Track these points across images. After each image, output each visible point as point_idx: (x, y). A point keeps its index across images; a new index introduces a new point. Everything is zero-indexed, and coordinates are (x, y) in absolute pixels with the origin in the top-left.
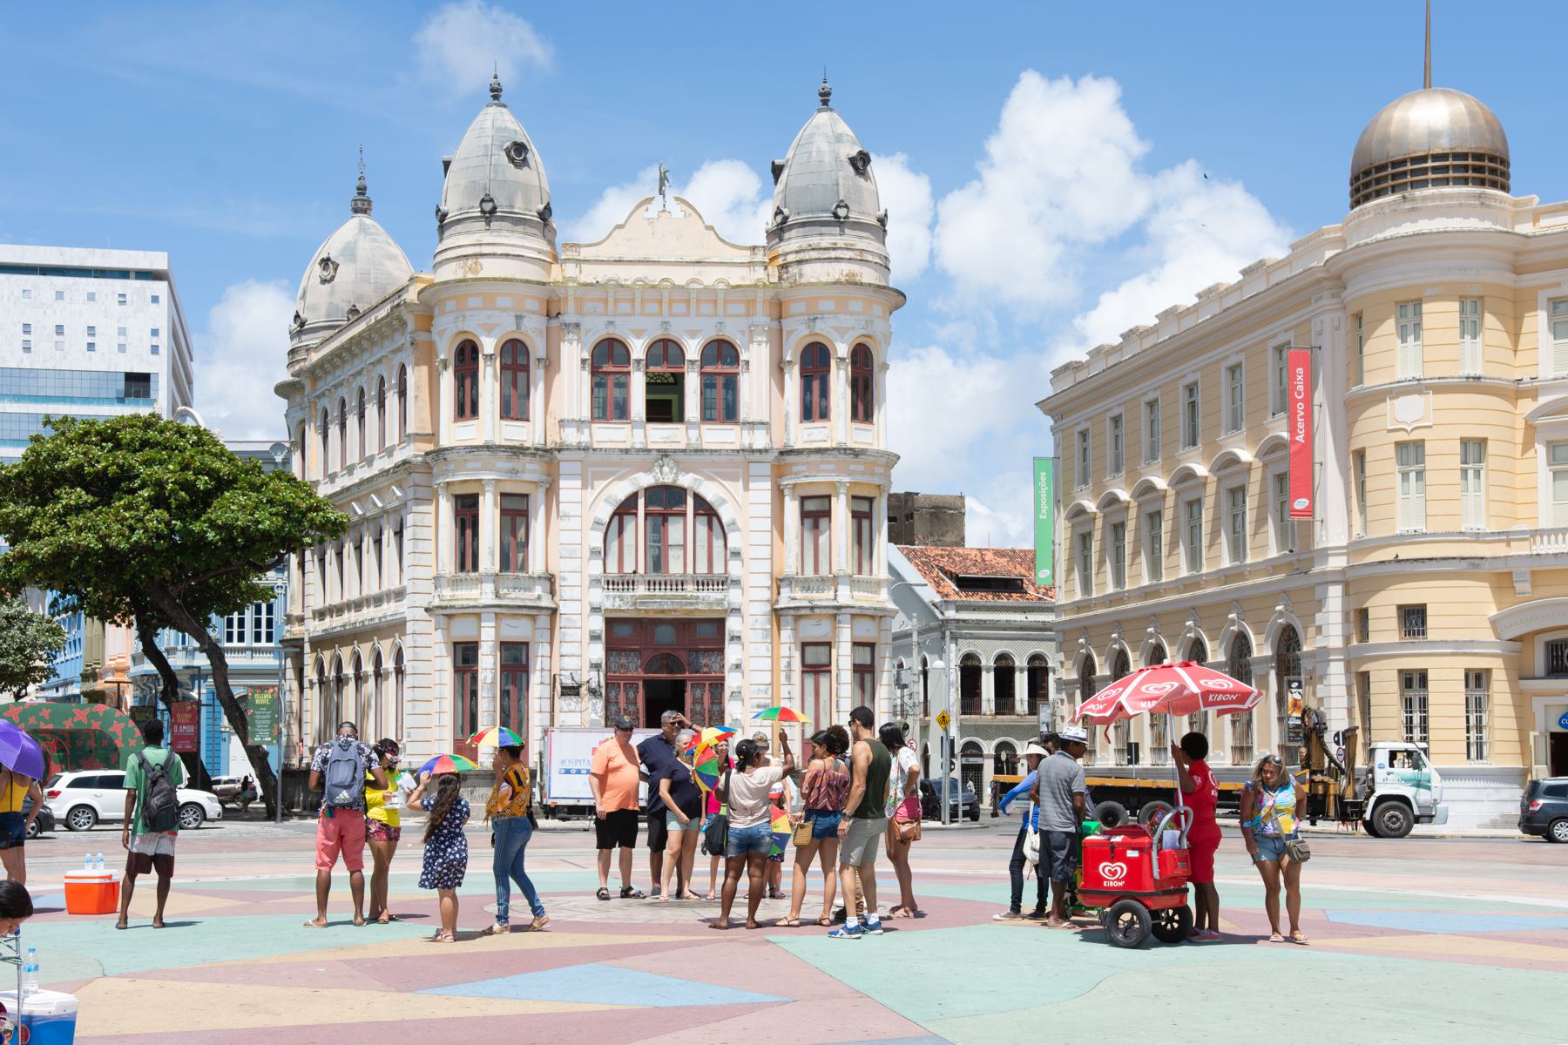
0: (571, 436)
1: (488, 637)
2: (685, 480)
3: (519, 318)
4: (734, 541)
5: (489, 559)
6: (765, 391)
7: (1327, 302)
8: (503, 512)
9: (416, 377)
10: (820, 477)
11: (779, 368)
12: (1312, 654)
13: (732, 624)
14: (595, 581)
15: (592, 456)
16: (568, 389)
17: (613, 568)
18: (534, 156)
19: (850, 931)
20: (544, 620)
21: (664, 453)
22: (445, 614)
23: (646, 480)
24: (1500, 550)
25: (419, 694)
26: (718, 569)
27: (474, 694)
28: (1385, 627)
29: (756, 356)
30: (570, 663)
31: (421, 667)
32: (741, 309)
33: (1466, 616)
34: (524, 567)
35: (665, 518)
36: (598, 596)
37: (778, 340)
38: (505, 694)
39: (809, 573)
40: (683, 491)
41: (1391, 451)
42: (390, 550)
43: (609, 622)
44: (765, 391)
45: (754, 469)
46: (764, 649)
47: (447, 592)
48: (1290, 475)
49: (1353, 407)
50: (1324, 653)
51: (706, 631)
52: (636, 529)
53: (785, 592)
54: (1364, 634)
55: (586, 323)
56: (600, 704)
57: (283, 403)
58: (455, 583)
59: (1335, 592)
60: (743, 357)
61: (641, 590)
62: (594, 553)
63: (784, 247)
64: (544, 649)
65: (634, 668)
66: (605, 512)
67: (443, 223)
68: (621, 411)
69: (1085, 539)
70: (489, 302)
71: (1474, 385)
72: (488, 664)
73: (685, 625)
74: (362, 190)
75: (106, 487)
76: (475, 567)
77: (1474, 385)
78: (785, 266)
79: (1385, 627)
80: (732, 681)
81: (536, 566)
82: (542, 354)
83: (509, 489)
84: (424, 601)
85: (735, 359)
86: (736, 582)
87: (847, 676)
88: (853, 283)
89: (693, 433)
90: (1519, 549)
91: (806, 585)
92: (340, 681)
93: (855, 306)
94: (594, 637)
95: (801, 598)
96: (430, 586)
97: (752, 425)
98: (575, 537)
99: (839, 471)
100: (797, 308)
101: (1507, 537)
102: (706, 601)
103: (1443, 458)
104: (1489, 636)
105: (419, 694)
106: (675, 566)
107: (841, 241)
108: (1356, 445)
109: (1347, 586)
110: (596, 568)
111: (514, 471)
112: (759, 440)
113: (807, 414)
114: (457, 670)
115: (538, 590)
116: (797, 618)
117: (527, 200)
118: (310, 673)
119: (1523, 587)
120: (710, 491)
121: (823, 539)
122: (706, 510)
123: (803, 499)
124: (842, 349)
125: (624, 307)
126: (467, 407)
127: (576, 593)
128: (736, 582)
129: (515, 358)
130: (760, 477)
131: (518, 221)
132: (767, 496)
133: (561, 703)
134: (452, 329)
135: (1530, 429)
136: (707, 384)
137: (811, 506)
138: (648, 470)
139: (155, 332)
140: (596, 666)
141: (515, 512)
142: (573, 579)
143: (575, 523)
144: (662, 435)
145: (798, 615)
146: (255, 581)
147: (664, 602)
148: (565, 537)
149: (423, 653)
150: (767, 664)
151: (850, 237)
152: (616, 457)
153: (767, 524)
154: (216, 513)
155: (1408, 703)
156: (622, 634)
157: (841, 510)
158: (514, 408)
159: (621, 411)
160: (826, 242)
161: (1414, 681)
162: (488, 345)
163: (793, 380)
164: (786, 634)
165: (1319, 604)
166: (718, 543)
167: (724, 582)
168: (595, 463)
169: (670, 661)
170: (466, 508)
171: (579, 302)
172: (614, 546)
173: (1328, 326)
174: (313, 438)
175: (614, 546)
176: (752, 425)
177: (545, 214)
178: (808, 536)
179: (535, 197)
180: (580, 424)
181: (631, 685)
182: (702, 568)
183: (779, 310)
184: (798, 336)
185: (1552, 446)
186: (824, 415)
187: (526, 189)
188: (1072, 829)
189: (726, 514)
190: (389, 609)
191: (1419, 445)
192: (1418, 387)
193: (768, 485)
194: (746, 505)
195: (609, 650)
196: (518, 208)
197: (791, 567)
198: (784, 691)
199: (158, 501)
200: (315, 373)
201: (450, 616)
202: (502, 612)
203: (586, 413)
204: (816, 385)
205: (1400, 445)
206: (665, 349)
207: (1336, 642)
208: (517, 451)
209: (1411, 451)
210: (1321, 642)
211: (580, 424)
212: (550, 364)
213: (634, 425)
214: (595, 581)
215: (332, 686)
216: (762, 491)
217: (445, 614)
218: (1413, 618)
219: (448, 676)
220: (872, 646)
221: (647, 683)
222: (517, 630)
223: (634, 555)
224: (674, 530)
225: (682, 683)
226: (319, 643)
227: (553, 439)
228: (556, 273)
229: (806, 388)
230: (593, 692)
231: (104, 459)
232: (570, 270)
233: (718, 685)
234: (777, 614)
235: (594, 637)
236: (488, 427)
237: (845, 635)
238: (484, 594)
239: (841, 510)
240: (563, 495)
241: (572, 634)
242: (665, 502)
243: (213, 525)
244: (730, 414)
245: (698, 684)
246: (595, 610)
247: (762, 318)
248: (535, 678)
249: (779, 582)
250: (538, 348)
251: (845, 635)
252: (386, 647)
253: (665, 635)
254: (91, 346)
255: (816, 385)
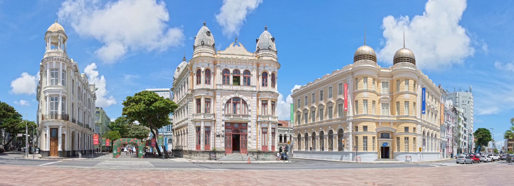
0: (219, 87)
1: (202, 125)
2: (240, 96)
3: (209, 64)
4: (249, 108)
5: (203, 111)
6: (255, 81)
7: (350, 76)
8: (205, 102)
9: (190, 78)
10: (267, 96)
11: (258, 76)
12: (346, 133)
13: (249, 124)
14: (223, 115)
15: (223, 91)
16: (217, 79)
17: (226, 113)
18: (211, 34)
20: (213, 123)
21: (236, 91)
22: (194, 121)
23: (233, 96)
24: (377, 118)
25: (190, 137)
26: (246, 113)
27: (200, 136)
28: (361, 130)
29: (254, 73)
30: (218, 131)
31: (191, 132)
32: (251, 64)
33: (372, 128)
34: (209, 112)
35: (236, 103)
36: (223, 118)
37: (258, 71)
38: (206, 136)
39: (263, 115)
40: (240, 98)
41: (362, 101)
42: (186, 112)
43: (226, 123)
44: (255, 81)
45: (253, 95)
46: (255, 129)
47: (195, 117)
48: (341, 105)
49: (354, 94)
50: (349, 133)
51: (244, 125)
52: (231, 105)
53: (259, 118)
54: (357, 130)
55: (222, 66)
56: (224, 138)
58: (196, 115)
59: (351, 123)
60: (251, 73)
61: (232, 117)
62: (223, 110)
63: (259, 54)
64: (213, 128)
65: (230, 132)
66: (225, 102)
67: (194, 47)
68: (228, 83)
69: (299, 116)
70: (203, 61)
71: (374, 92)
72: (202, 130)
73: (240, 124)
75: (137, 102)
76: (200, 112)
77: (374, 92)
78: (259, 57)
79: (361, 130)
80: (249, 134)
81: (212, 112)
82: (213, 71)
83: (207, 97)
84: (191, 120)
85: (250, 74)
86: (250, 116)
87: (271, 134)
88: (272, 60)
89: (242, 88)
90: (380, 118)
91: (263, 117)
92: (179, 135)
93: (272, 65)
94: (223, 126)
95: (262, 119)
96: (192, 117)
97: (253, 86)
98: (219, 107)
99: (269, 96)
100: (262, 65)
101: (378, 116)
102: (244, 119)
103: (370, 103)
104: (375, 131)
105: (190, 137)
106: (238, 113)
107: (270, 53)
108: (356, 99)
109: (353, 122)
110: (223, 112)
111: (207, 94)
112: (254, 89)
113: (263, 85)
114: (197, 132)
115: (212, 117)
116: (261, 123)
117: (210, 42)
118: (175, 134)
119: (380, 124)
120: (245, 98)
121: (266, 108)
122: (244, 102)
123: (262, 101)
124: (270, 73)
125: (229, 63)
126: (199, 82)
127: (219, 117)
128: (250, 116)
129: (208, 72)
130: (254, 96)
131: (208, 46)
132: (256, 100)
133: (216, 138)
134: (196, 67)
135: (379, 100)
136: (245, 78)
137: (264, 102)
138: (233, 94)
140: (223, 131)
141: (208, 101)
142: (219, 115)
143: (219, 104)
144: (236, 88)
145: (261, 122)
147: (236, 119)
148: (217, 107)
149: (191, 129)
150: (255, 131)
151: (271, 53)
152: (227, 91)
153: (256, 105)
154: (154, 105)
155: (364, 142)
156: (228, 125)
157: (269, 103)
158: (208, 82)
159: (228, 83)
160: (267, 53)
161: (365, 138)
162: (203, 69)
163: (261, 79)
164: (259, 126)
165: (348, 125)
166: (246, 109)
167: (248, 116)
168: (223, 93)
169: (237, 131)
170: (199, 101)
171: (220, 61)
172: (227, 108)
173: (350, 80)
174: (175, 96)
175: (227, 108)
176: (253, 86)
177: (214, 45)
178: (263, 108)
179: (212, 42)
180: (220, 85)
181: (230, 135)
182: (243, 113)
183: (258, 65)
184: (262, 70)
185: (382, 104)
186: (266, 85)
187: (210, 40)
188: (110, 145)
189: (248, 103)
190: (186, 122)
191: (367, 100)
192: (367, 91)
193: (256, 98)
194: (252, 101)
195: (225, 128)
196: (209, 43)
197: (260, 113)
198: (259, 137)
199: (144, 103)
201: (195, 122)
202: (205, 121)
203: (221, 83)
204: (265, 79)
205: (364, 100)
206: (237, 71)
207: (351, 131)
208: (208, 90)
209: (365, 101)
210: (348, 131)
211: (220, 85)
212: (214, 74)
213: (231, 85)
214: (223, 115)
215: (178, 136)
216: (255, 98)
217: (194, 121)
218: (365, 128)
219: (195, 133)
220: (274, 129)
221: (233, 135)
222: (208, 124)
223: (231, 111)
224: (238, 106)
225: (239, 135)
226: (176, 129)
227: (215, 88)
228: (216, 56)
229: (263, 80)
230: (223, 136)
231: (138, 97)
232: (218, 55)
233: (246, 135)
234: (257, 122)
235: (223, 126)
236: (203, 85)
237: (270, 126)
238: (202, 117)
239: (269, 103)
240: (217, 99)
241: (219, 125)
242: (236, 101)
243: (153, 107)
244: (249, 84)
245: (242, 135)
246: (223, 121)
247: (255, 66)
248: (211, 133)
249: (258, 116)
250: (212, 71)
251: (270, 126)
252: (185, 129)
253: (236, 126)
255: (265, 79)
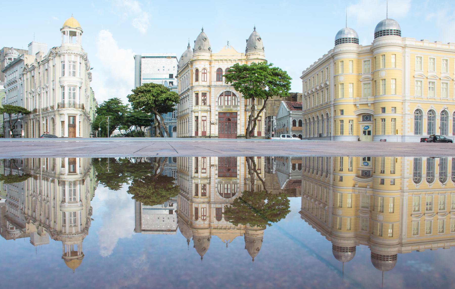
13: (238, 113)
19: (77, 180)
51: (234, 114)
53: (13, 115)
57: (302, 80)
66: (218, 95)
74: (189, 45)
102: (234, 110)
139: (174, 67)
146: (130, 107)
156: (221, 115)
162: (200, 70)
200: (180, 73)
254: (164, 70)
